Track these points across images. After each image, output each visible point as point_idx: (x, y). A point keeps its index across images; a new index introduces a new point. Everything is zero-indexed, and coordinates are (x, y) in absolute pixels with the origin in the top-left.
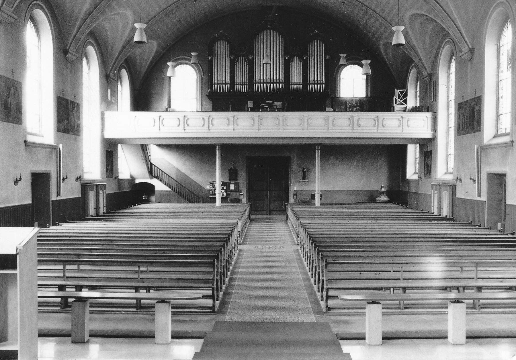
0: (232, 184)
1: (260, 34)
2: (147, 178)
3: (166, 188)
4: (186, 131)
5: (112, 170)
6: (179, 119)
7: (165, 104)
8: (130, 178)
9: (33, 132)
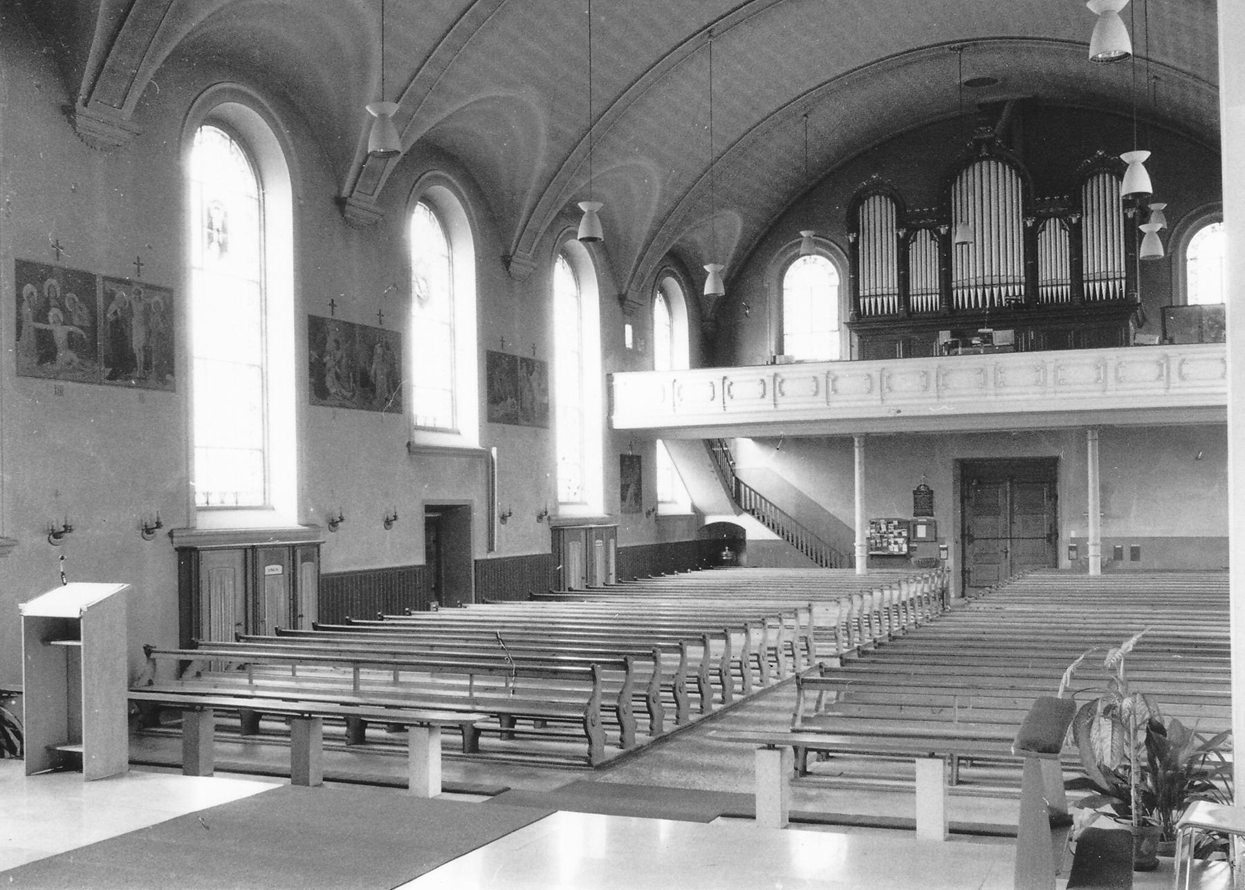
0: (922, 524)
1: (965, 171)
2: (727, 514)
3: (769, 535)
4: (780, 407)
5: (638, 496)
6: (763, 381)
7: (771, 346)
8: (693, 513)
9: (437, 426)
